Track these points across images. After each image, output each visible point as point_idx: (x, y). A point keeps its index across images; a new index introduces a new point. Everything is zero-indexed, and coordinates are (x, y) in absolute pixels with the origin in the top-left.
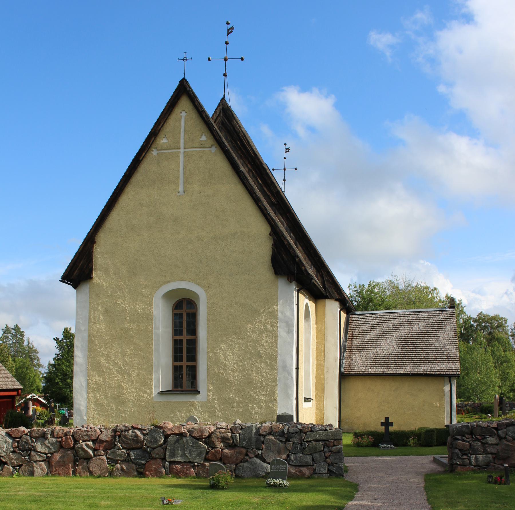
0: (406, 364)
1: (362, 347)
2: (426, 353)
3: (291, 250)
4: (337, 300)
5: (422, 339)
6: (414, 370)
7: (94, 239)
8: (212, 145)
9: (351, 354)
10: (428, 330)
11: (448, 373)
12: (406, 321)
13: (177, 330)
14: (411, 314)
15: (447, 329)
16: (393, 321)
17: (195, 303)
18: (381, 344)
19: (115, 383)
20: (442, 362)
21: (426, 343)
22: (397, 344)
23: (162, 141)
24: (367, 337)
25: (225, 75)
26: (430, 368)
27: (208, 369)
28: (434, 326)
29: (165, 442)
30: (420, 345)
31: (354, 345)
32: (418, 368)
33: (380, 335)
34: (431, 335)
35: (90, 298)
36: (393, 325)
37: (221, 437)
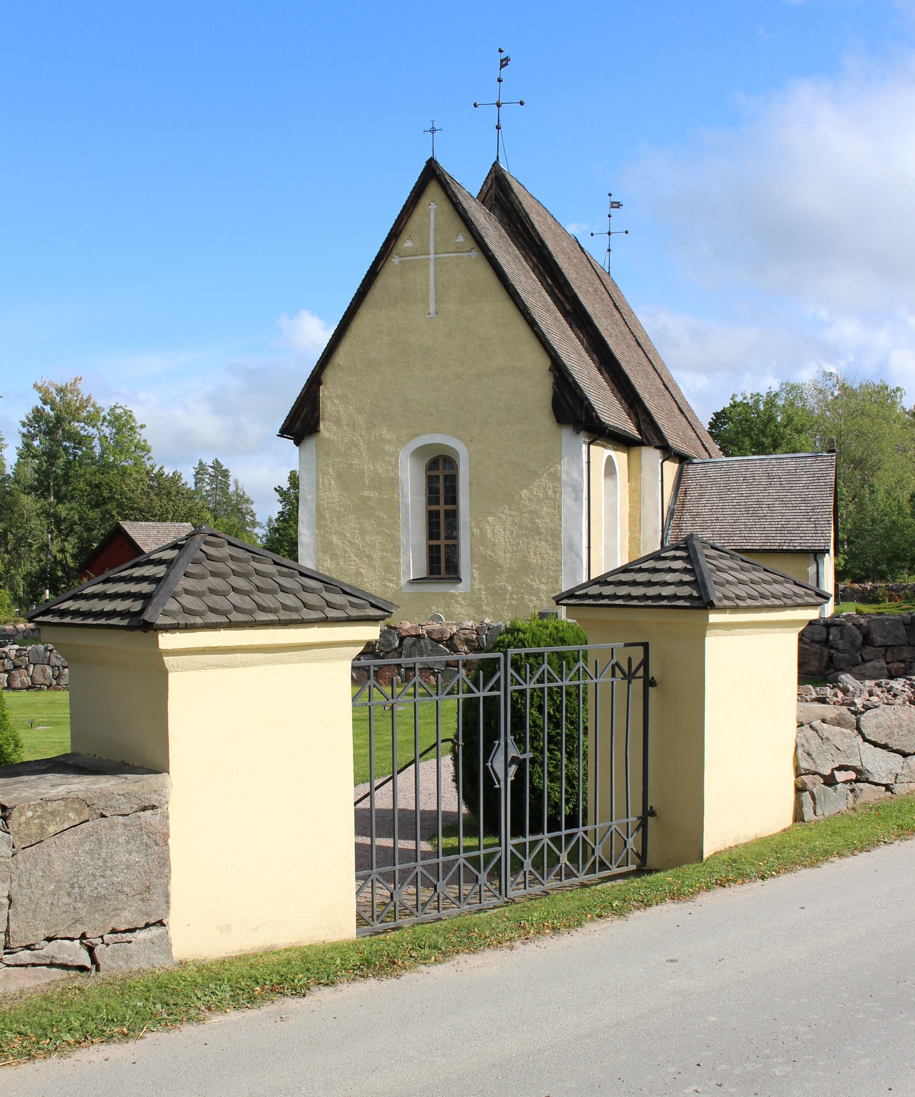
0: (756, 535)
1: (697, 511)
2: (785, 520)
3: (578, 391)
4: (657, 447)
5: (782, 500)
6: (766, 544)
7: (321, 380)
8: (472, 249)
9: (681, 522)
10: (794, 485)
11: (813, 548)
12: (764, 472)
13: (432, 495)
14: (772, 461)
15: (820, 484)
16: (744, 473)
17: (455, 461)
18: (725, 507)
19: (352, 569)
20: (806, 532)
21: (788, 505)
22: (747, 506)
23: (406, 245)
24: (706, 497)
25: (498, 128)
26: (788, 541)
27: (472, 549)
28: (803, 479)
29: (400, 644)
30: (778, 508)
31: (686, 509)
32: (771, 541)
33: (724, 493)
34: (796, 494)
35: (317, 457)
36: (744, 478)
37: (465, 639)
